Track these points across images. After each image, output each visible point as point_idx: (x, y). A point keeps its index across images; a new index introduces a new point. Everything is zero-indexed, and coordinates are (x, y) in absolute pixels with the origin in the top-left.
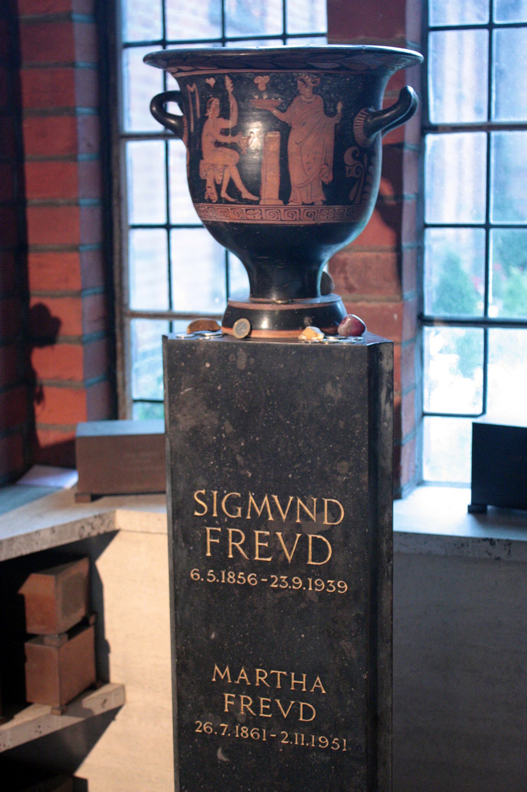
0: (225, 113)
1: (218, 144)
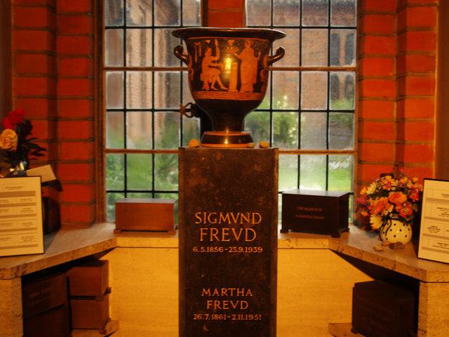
0: (214, 54)
1: (210, 67)
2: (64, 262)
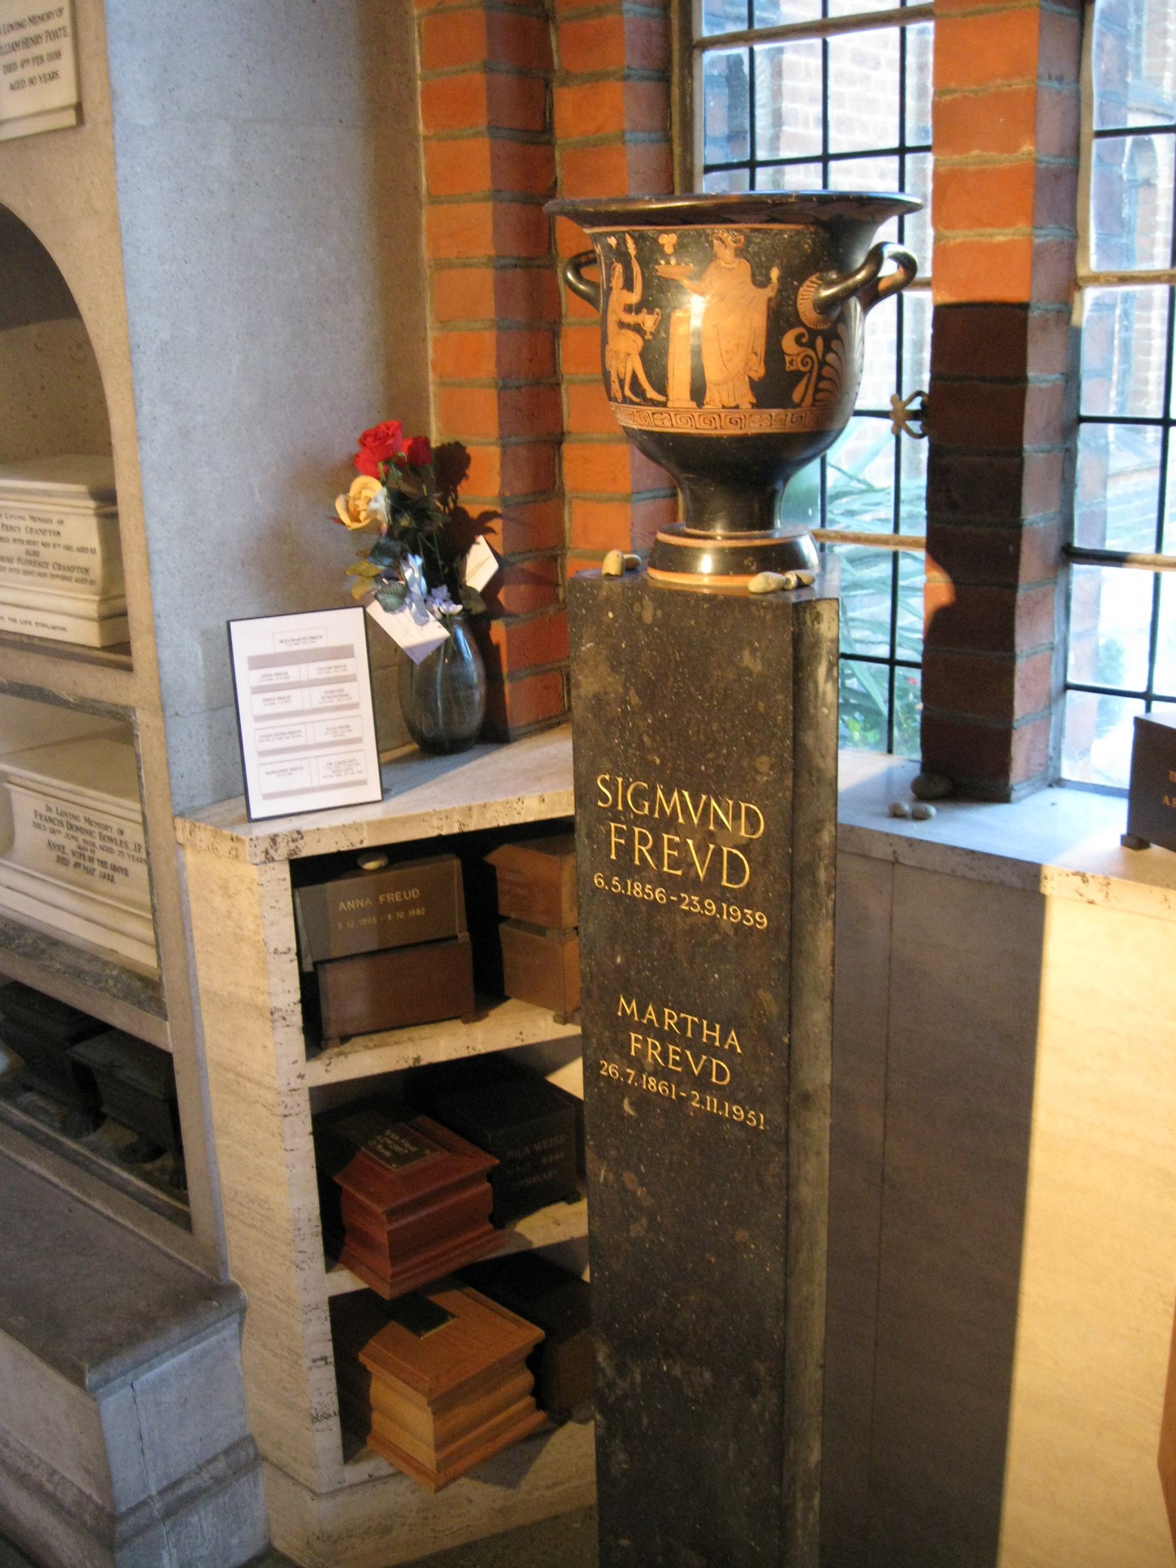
2: (433, 833)
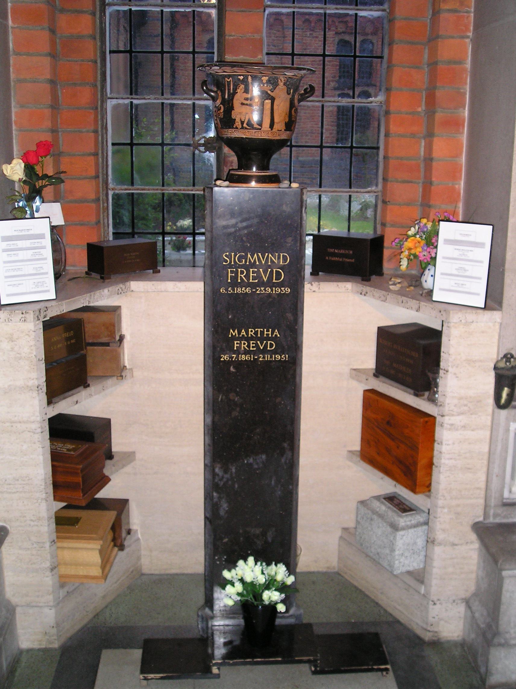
1: (243, 104)
